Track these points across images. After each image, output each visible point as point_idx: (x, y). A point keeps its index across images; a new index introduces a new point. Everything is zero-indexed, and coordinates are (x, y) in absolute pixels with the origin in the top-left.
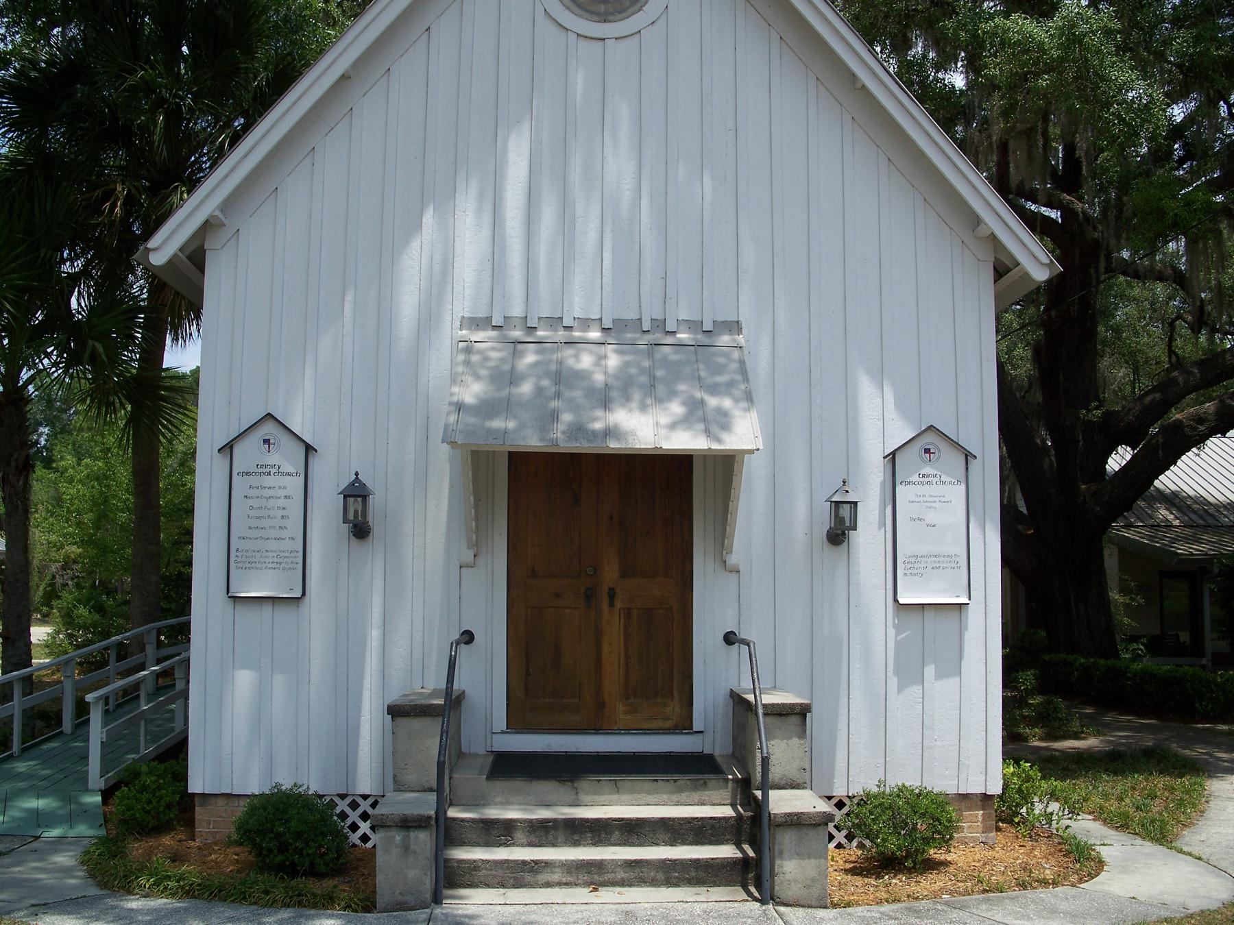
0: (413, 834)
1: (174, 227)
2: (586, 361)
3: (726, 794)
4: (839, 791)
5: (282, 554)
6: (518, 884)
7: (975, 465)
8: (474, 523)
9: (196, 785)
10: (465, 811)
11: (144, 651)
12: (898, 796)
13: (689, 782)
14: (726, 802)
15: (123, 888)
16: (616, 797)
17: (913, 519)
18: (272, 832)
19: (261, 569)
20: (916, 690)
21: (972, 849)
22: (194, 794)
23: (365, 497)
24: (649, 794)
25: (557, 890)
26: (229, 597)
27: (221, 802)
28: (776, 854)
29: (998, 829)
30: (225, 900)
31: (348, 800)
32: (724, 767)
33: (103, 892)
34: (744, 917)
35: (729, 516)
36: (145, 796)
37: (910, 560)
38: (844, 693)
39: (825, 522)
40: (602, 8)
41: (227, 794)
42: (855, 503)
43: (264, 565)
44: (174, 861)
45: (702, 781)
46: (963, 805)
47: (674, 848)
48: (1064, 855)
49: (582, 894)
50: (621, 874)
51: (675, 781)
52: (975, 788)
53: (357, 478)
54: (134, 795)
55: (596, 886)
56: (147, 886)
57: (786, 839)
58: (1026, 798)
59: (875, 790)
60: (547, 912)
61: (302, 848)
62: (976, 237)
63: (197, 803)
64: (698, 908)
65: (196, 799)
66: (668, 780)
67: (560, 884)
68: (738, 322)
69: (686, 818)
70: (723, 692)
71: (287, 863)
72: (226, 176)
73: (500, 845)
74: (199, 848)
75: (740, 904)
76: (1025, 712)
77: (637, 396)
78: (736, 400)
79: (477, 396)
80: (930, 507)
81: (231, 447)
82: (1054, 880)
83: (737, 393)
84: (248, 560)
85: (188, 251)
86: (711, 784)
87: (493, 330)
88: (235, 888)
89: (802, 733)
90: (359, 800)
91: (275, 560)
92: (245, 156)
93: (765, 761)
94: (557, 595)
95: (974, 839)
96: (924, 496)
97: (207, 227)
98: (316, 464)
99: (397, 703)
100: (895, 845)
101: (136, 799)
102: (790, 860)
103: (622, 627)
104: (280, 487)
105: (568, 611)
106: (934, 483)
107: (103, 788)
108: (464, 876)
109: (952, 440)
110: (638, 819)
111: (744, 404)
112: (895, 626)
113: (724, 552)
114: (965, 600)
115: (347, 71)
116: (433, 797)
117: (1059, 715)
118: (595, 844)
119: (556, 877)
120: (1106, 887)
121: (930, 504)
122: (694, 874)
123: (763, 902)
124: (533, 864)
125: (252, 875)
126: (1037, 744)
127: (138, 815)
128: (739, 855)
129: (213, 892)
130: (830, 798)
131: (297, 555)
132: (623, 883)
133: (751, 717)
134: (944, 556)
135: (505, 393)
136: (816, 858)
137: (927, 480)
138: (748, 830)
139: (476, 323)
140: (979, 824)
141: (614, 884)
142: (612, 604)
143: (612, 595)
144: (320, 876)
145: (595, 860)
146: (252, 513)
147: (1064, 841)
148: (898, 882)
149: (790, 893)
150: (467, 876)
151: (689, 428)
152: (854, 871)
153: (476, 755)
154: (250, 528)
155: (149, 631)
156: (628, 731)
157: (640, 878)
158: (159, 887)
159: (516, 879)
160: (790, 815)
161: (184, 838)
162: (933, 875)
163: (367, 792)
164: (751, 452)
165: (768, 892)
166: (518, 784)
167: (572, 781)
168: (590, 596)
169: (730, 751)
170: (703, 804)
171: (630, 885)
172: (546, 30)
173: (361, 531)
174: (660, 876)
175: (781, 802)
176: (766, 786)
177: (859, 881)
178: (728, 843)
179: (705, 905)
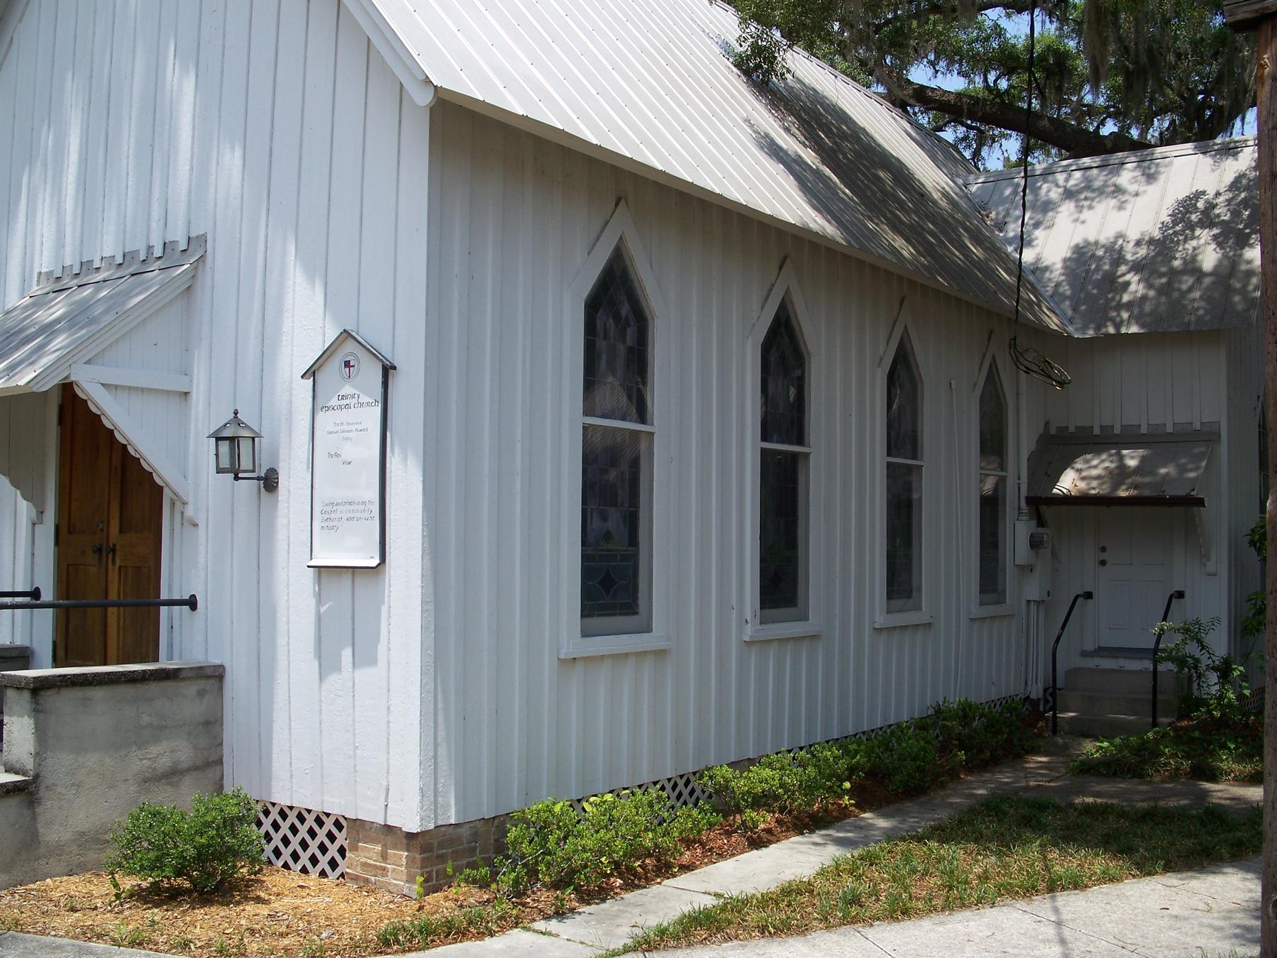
17: (330, 455)
96: (342, 424)
121: (346, 435)
134: (358, 503)
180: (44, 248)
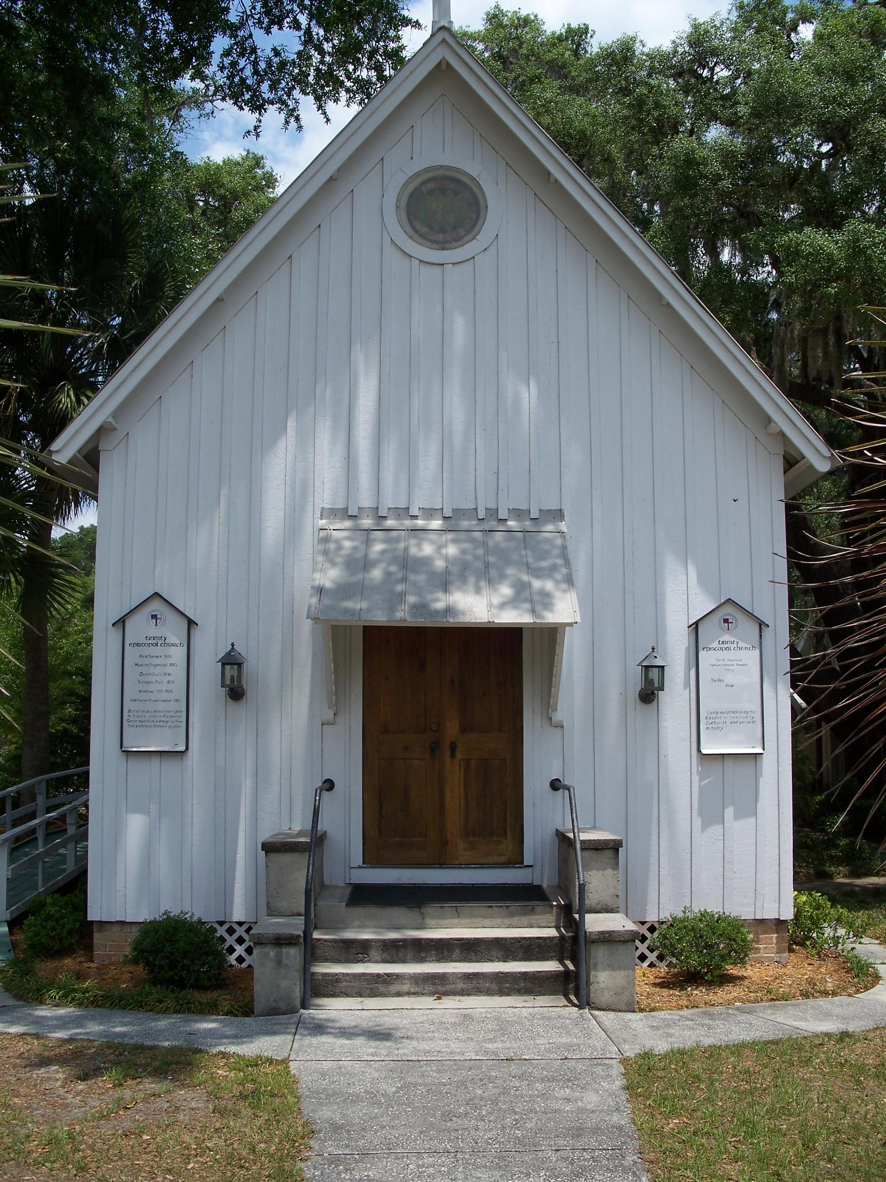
0: (285, 950)
1: (74, 432)
2: (427, 549)
3: (551, 918)
4: (652, 917)
5: (168, 714)
6: (374, 994)
7: (768, 633)
8: (334, 686)
9: (93, 914)
10: (326, 934)
11: (35, 800)
12: (701, 920)
13: (519, 908)
14: (551, 925)
15: (36, 999)
16: (456, 921)
18: (163, 952)
19: (150, 726)
20: (717, 829)
21: (767, 967)
22: (92, 922)
23: (240, 665)
24: (485, 918)
25: (406, 998)
26: (123, 751)
27: (116, 928)
28: (592, 966)
29: (791, 950)
30: (124, 1009)
31: (226, 926)
32: (550, 897)
33: (20, 1003)
34: (564, 1018)
35: (554, 679)
36: (50, 924)
37: (712, 716)
38: (654, 832)
39: (636, 684)
40: (441, 237)
41: (121, 922)
42: (663, 667)
43: (153, 724)
44: (78, 978)
45: (530, 907)
46: (760, 929)
47: (506, 963)
48: (846, 972)
49: (428, 1002)
50: (460, 985)
51: (507, 907)
52: (770, 914)
53: (233, 648)
54: (41, 923)
55: (440, 995)
56: (57, 998)
57: (600, 953)
58: (816, 923)
59: (681, 915)
60: (398, 1015)
61: (189, 966)
62: (767, 433)
63: (95, 930)
64: (525, 1012)
65: (95, 926)
66: (501, 906)
67: (409, 994)
68: (561, 510)
69: (517, 938)
70: (550, 831)
71: (176, 978)
72: (118, 387)
73: (358, 962)
74: (97, 968)
75: (562, 1009)
76: (833, 852)
77: (472, 580)
78: (557, 582)
79: (333, 581)
80: (728, 670)
81: (124, 622)
82: (833, 991)
83: (558, 576)
84: (139, 719)
85: (84, 452)
86: (538, 909)
87: (349, 519)
88: (133, 998)
89: (615, 866)
90: (236, 927)
91: (162, 719)
92: (134, 370)
93: (582, 887)
94: (406, 748)
95: (770, 959)
97: (102, 431)
98: (197, 636)
99: (270, 840)
100: (696, 961)
101: (42, 927)
102: (603, 971)
103: (462, 776)
104: (166, 656)
105: (416, 762)
106: (732, 649)
107: (9, 919)
108: (327, 987)
109: (747, 611)
110: (475, 939)
111: (564, 586)
112: (698, 773)
113: (550, 710)
114: (760, 751)
115: (221, 295)
116: (301, 920)
117: (863, 855)
118: (439, 961)
119: (405, 988)
120: (878, 997)
121: (728, 667)
122: (523, 985)
123: (580, 1007)
124: (386, 977)
125: (147, 987)
126: (840, 880)
127: (43, 941)
128: (562, 968)
129: (114, 1002)
130: (643, 923)
131: (180, 714)
132: (462, 993)
133: (571, 850)
135: (360, 577)
136: (625, 969)
137: (726, 646)
138: (569, 948)
139: (333, 513)
140: (774, 945)
141: (454, 993)
142: (453, 756)
143: (453, 748)
144: (205, 989)
145: (439, 973)
146: (142, 679)
147: (847, 960)
148: (698, 993)
149: (603, 999)
150: (330, 987)
151: (515, 608)
152: (662, 985)
153: (336, 887)
154: (140, 691)
155: (39, 783)
156: (468, 865)
157: (477, 988)
158: (67, 996)
159: (371, 989)
160: (603, 933)
161: (84, 960)
162: (729, 988)
163: (242, 920)
164: (571, 625)
165: (585, 999)
166: (373, 910)
167: (419, 907)
168: (434, 748)
169: (556, 883)
170: (531, 927)
171: (469, 995)
172: (391, 253)
173: (236, 693)
174: (494, 986)
175: (595, 923)
176: (583, 911)
177: (665, 992)
178: (552, 960)
179: (532, 1010)
180: (360, 1041)
